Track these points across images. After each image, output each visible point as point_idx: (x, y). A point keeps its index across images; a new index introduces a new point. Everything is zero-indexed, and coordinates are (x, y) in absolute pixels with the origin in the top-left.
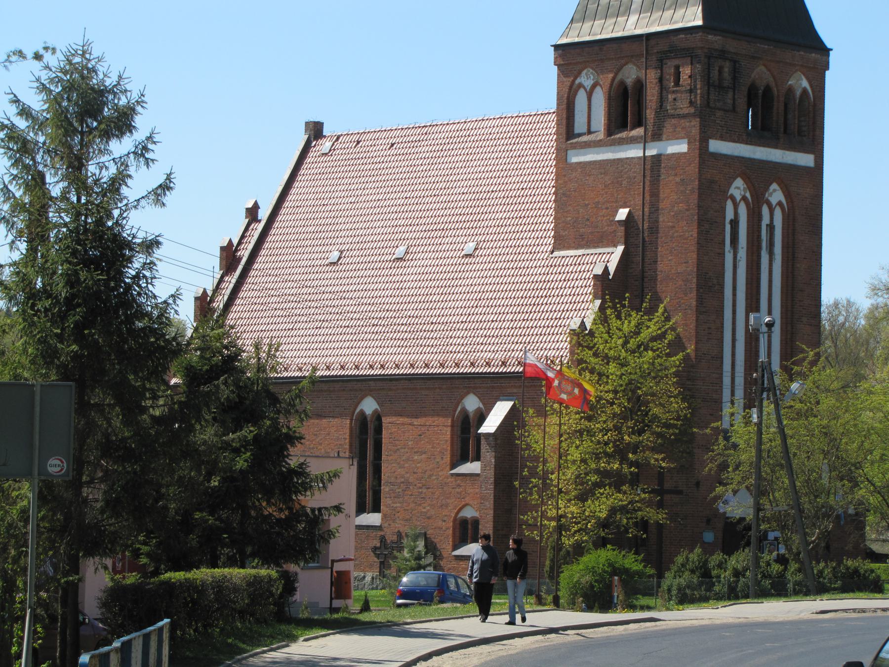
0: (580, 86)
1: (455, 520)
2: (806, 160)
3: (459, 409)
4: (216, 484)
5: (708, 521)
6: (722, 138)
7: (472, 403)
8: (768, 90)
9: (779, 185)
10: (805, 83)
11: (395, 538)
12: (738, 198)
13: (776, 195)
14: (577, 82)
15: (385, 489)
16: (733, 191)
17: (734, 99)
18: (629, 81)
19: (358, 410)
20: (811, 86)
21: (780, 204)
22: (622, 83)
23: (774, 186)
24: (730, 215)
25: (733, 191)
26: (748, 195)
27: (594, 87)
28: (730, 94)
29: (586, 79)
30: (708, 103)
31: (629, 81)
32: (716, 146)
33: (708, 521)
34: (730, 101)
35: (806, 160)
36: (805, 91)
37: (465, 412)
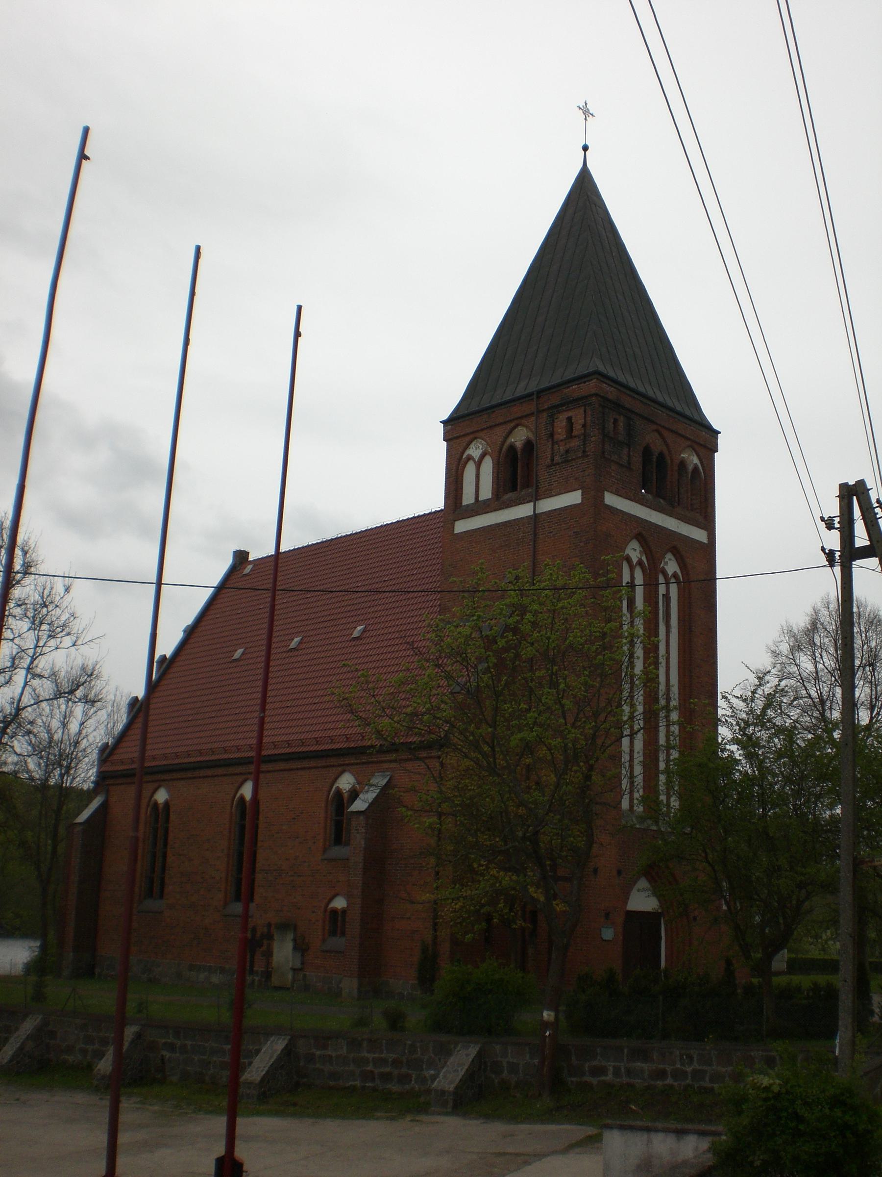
0: (470, 458)
1: (325, 911)
2: (699, 535)
3: (333, 789)
4: (759, 956)
5: (607, 915)
6: (617, 493)
7: (346, 782)
8: (661, 455)
9: (674, 555)
10: (696, 460)
11: (265, 930)
12: (635, 560)
13: (671, 566)
14: (468, 452)
15: (259, 877)
16: (629, 551)
17: (629, 456)
18: (519, 445)
19: (238, 795)
20: (702, 463)
21: (675, 575)
22: (512, 448)
23: (669, 556)
24: (626, 578)
25: (629, 551)
26: (644, 559)
27: (483, 456)
28: (625, 451)
29: (475, 451)
30: (603, 453)
31: (519, 445)
32: (610, 499)
33: (607, 915)
34: (625, 457)
35: (699, 535)
36: (696, 468)
37: (339, 792)
